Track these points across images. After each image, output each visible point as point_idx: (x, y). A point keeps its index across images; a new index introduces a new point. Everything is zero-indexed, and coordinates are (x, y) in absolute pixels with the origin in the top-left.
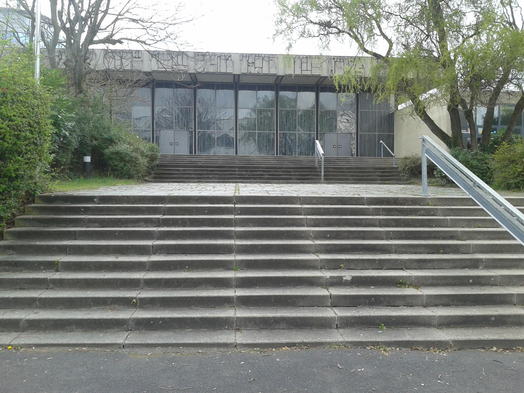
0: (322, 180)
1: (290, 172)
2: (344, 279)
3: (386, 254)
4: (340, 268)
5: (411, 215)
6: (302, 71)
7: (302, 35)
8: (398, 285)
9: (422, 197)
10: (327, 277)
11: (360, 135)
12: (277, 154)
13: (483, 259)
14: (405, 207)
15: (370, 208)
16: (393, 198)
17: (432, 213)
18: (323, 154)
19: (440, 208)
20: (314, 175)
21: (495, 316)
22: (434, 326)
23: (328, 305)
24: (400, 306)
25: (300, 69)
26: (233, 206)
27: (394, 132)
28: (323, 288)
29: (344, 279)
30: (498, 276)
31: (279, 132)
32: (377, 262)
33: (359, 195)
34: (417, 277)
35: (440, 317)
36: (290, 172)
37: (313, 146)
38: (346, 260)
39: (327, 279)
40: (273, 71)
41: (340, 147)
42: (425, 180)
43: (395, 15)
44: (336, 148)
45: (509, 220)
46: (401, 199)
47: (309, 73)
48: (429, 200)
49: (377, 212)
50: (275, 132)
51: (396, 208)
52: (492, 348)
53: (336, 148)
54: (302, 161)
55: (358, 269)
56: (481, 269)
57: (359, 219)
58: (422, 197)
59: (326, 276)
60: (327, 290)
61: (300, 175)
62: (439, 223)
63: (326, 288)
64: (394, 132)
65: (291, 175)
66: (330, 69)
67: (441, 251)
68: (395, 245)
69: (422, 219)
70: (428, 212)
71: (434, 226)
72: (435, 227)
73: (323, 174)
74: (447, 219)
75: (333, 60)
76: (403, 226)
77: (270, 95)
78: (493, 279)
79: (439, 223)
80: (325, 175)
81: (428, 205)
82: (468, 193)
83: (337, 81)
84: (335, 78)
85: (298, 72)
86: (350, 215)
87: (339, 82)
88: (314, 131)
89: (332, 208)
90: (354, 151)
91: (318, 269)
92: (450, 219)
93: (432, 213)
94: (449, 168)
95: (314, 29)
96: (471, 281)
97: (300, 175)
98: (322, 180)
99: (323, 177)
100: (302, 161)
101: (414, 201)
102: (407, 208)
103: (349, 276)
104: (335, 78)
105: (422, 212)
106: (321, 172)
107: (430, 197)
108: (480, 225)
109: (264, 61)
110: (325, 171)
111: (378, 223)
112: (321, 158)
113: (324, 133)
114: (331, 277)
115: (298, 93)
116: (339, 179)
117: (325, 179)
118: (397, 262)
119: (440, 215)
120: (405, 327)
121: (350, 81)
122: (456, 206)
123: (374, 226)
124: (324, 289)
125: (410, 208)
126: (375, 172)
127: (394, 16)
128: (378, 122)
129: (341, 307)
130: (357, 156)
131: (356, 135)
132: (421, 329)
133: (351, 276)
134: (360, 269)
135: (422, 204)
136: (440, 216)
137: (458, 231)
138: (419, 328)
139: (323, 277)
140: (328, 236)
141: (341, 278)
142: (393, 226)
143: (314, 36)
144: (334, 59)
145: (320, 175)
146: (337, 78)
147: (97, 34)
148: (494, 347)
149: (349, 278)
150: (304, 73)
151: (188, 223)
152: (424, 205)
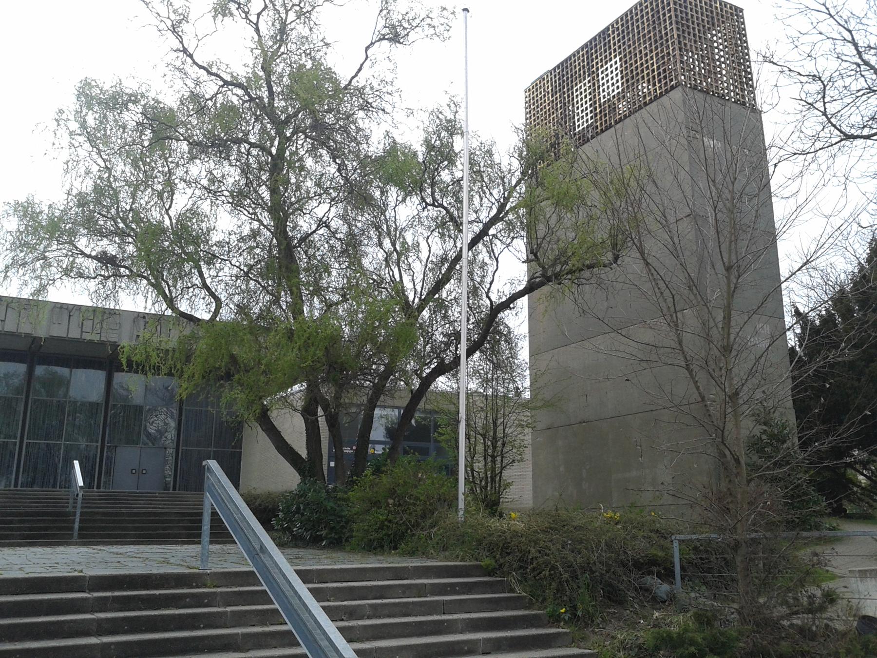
0: (75, 538)
1: (11, 522)
5: (166, 607)
6: (82, 332)
7: (67, 272)
9: (198, 571)
11: (182, 452)
12: (16, 485)
15: (89, 598)
17: (206, 601)
18: (81, 487)
19: (221, 592)
20: (60, 529)
25: (80, 329)
27: (241, 448)
31: (25, 441)
36: (11, 522)
37: (92, 470)
40: (25, 329)
41: (144, 472)
42: (205, 540)
43: (222, 259)
44: (137, 474)
45: (295, 610)
46: (156, 578)
47: (95, 338)
49: (102, 605)
50: (18, 441)
53: (137, 474)
54: (58, 499)
57: (58, 622)
58: (198, 571)
61: (30, 529)
62: (211, 621)
64: (241, 448)
65: (12, 529)
66: (136, 333)
69: (180, 615)
70: (198, 601)
71: (202, 626)
72: (204, 628)
73: (77, 526)
74: (226, 612)
75: (142, 319)
77: (21, 368)
79: (211, 621)
80: (80, 529)
81: (205, 586)
82: (251, 563)
83: (125, 355)
84: (122, 350)
85: (75, 334)
86: (47, 614)
87: (128, 357)
88: (97, 442)
89: (10, 602)
90: (170, 480)
93: (206, 601)
94: (233, 520)
95: (91, 265)
97: (30, 529)
98: (75, 538)
99: (76, 534)
100: (58, 499)
102: (160, 594)
104: (122, 350)
106: (73, 522)
107: (208, 571)
109: (9, 309)
110: (81, 521)
111: (95, 629)
112: (77, 495)
113: (116, 447)
115: (74, 370)
116: (110, 536)
117: (81, 536)
119: (221, 603)
121: (148, 357)
122: (254, 585)
123: (87, 634)
125: (165, 594)
126: (179, 521)
127: (220, 260)
128: (216, 428)
130: (174, 489)
131: (175, 450)
135: (194, 584)
136: (219, 607)
137: (237, 634)
142: (125, 632)
143: (88, 277)
144: (144, 317)
145: (72, 529)
146: (126, 350)
147: (525, 267)
150: (87, 337)
152: (198, 587)
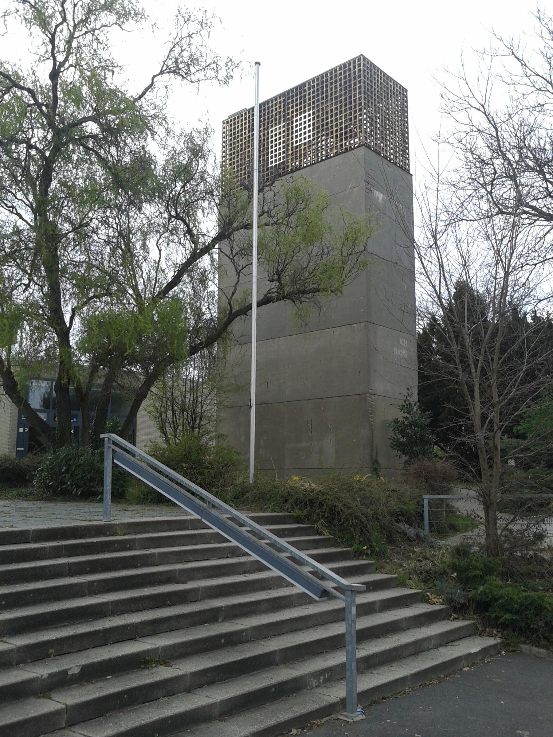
2: (70, 673)
3: (100, 618)
4: (48, 656)
8: (143, 666)
10: (44, 677)
13: (222, 607)
14: (95, 540)
16: (70, 528)
21: (274, 686)
22: (215, 719)
23: (61, 727)
24: (159, 699)
26: (203, 520)
28: (39, 698)
29: (70, 673)
30: (249, 628)
32: (101, 634)
33: (12, 526)
34: (166, 649)
35: (223, 702)
38: (57, 640)
39: (44, 680)
48: (117, 527)
49: (56, 553)
51: (82, 544)
52: (291, 732)
55: (73, 652)
56: (221, 622)
59: (42, 676)
60: (50, 699)
63: (44, 697)
67: (168, 602)
68: (112, 602)
76: (101, 571)
78: (244, 634)
91: (13, 666)
92: (159, 553)
96: (223, 641)
101: (99, 530)
103: (77, 666)
105: (116, 545)
108: (191, 559)
114: (51, 675)
118: (127, 629)
119: (138, 547)
120: (182, 730)
123: (61, 575)
124: (41, 701)
129: (82, 724)
132: (203, 726)
133: (80, 666)
134: (76, 652)
135: (108, 533)
137: (175, 570)
138: (200, 727)
139: (38, 678)
140: (3, 603)
141: (65, 672)
148: (293, 729)
149: (76, 671)
151: (278, 658)
